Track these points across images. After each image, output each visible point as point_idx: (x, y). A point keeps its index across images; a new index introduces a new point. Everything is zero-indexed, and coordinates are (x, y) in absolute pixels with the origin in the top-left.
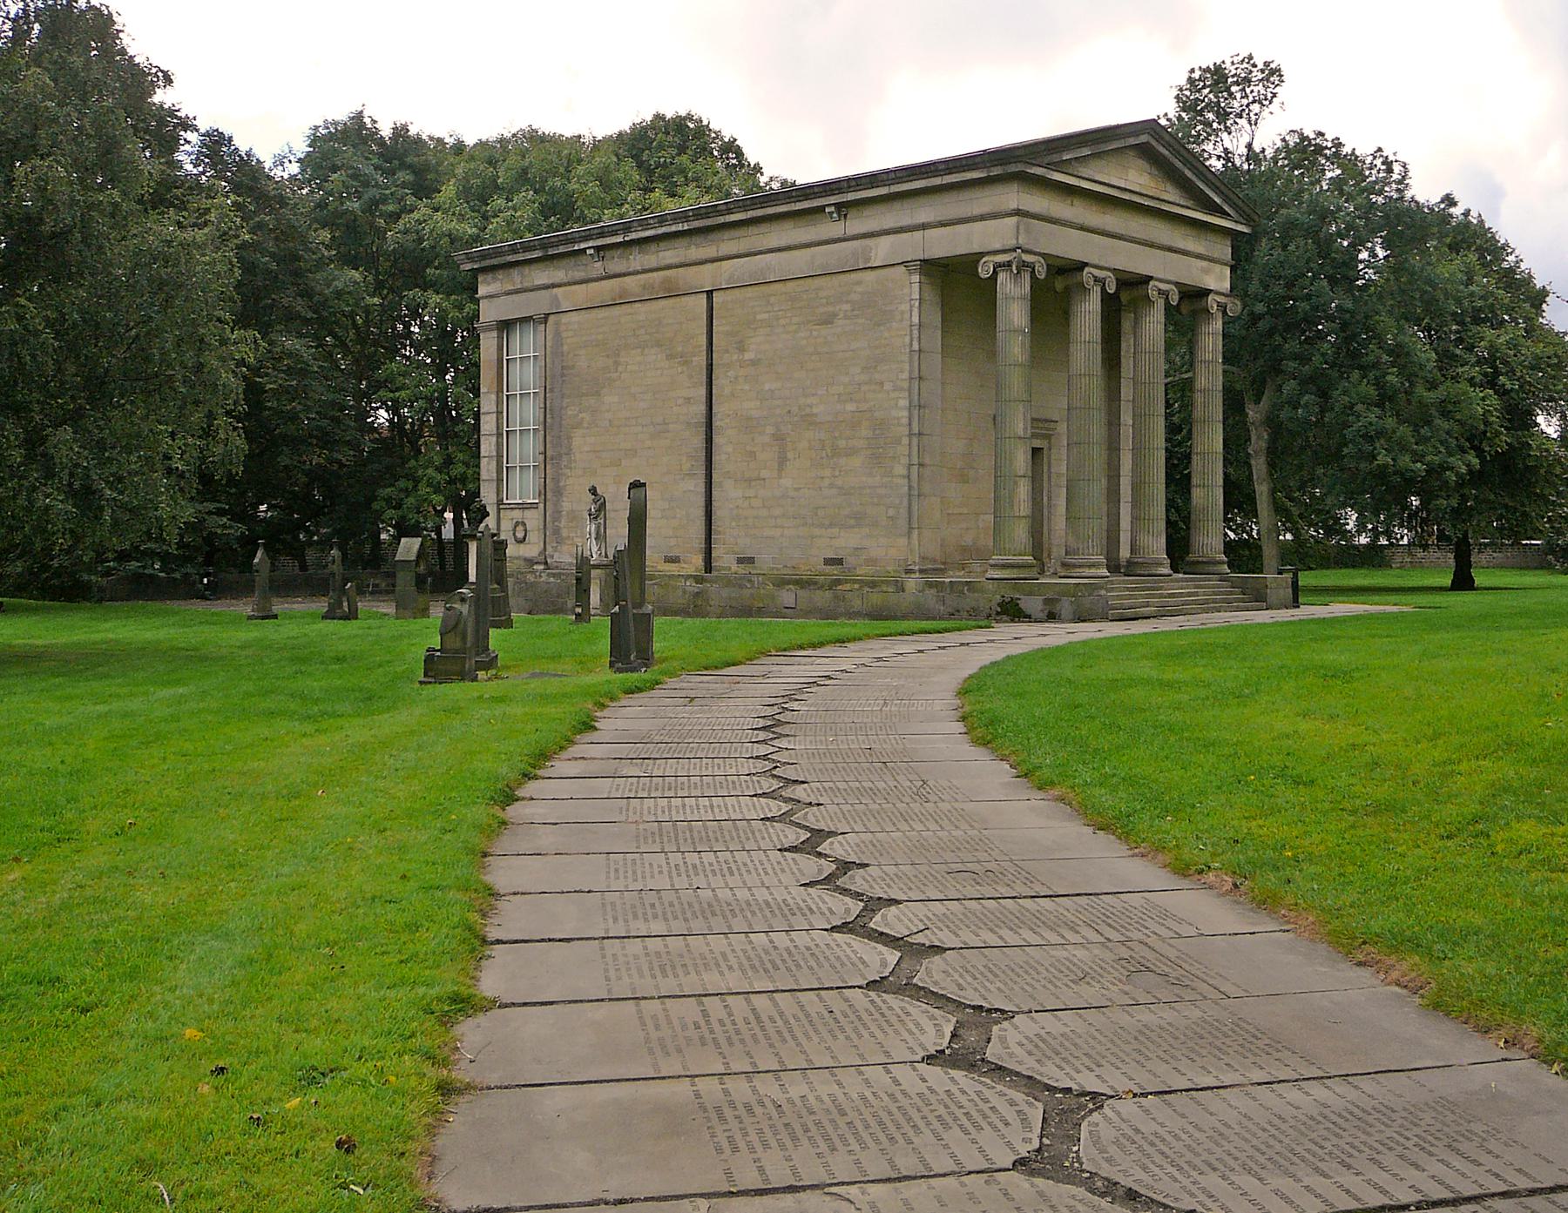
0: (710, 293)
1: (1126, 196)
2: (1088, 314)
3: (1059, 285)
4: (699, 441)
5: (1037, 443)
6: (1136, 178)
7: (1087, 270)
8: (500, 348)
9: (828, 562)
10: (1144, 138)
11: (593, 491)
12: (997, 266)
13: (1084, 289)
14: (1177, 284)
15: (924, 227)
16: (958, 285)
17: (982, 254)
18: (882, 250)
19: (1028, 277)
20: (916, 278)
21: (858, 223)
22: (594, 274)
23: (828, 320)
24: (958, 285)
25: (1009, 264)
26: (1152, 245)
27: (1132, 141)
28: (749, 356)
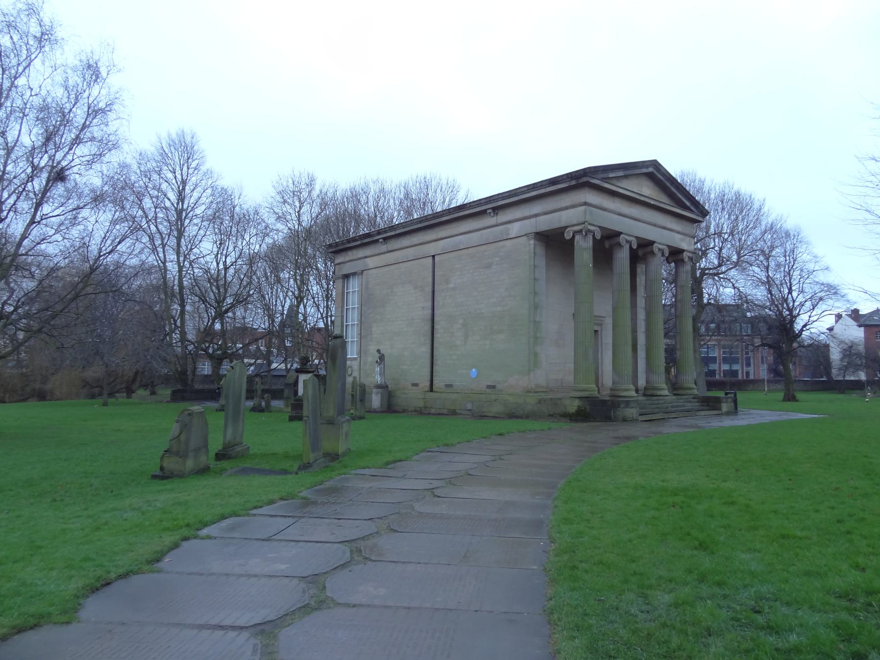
0: (433, 256)
1: (643, 199)
2: (622, 257)
3: (607, 244)
4: (428, 328)
5: (596, 328)
6: (646, 190)
7: (622, 236)
8: (343, 287)
9: (489, 387)
10: (651, 170)
11: (379, 351)
12: (575, 233)
13: (619, 245)
14: (668, 246)
15: (536, 216)
16: (555, 244)
17: (566, 227)
18: (515, 229)
19: (591, 237)
20: (532, 242)
21: (503, 217)
22: (382, 251)
23: (489, 266)
24: (555, 244)
25: (580, 231)
26: (655, 225)
27: (645, 170)
28: (451, 285)
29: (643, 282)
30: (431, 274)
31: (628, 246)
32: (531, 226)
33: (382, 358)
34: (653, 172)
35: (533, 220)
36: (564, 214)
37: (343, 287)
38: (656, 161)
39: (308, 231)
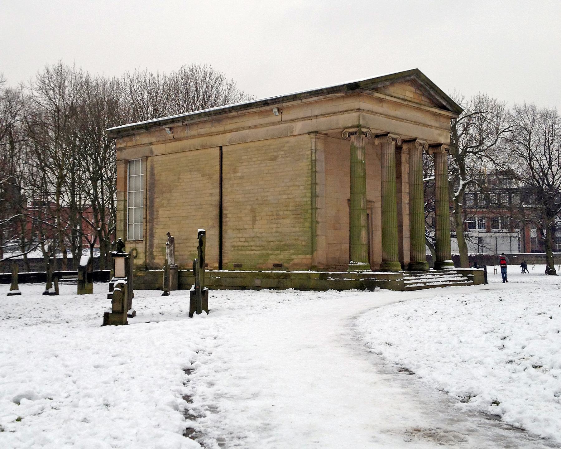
4: (216, 212)
8: (126, 172)
18: (298, 127)
23: (274, 159)
28: (239, 174)
29: (407, 169)
30: (219, 163)
31: (394, 142)
32: (311, 125)
33: (172, 240)
34: (414, 78)
35: (314, 121)
36: (342, 117)
37: (126, 172)
38: (417, 69)
39: (73, 108)
